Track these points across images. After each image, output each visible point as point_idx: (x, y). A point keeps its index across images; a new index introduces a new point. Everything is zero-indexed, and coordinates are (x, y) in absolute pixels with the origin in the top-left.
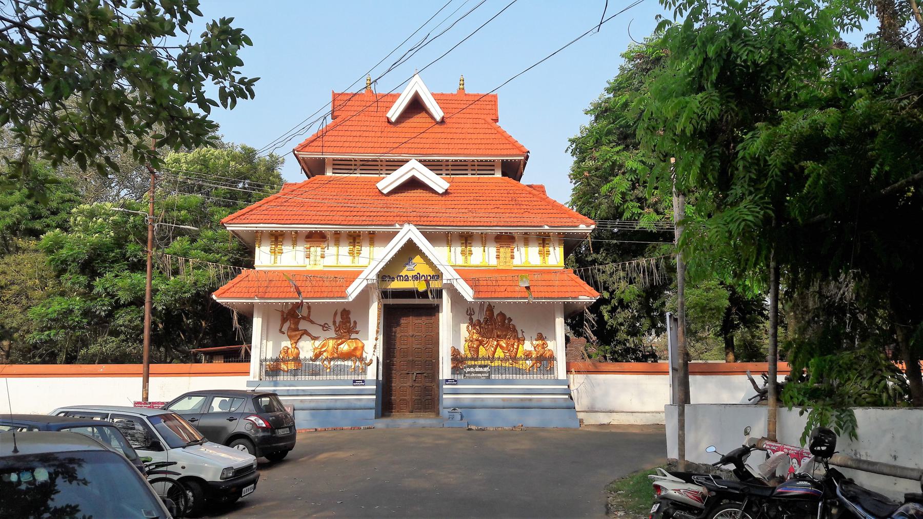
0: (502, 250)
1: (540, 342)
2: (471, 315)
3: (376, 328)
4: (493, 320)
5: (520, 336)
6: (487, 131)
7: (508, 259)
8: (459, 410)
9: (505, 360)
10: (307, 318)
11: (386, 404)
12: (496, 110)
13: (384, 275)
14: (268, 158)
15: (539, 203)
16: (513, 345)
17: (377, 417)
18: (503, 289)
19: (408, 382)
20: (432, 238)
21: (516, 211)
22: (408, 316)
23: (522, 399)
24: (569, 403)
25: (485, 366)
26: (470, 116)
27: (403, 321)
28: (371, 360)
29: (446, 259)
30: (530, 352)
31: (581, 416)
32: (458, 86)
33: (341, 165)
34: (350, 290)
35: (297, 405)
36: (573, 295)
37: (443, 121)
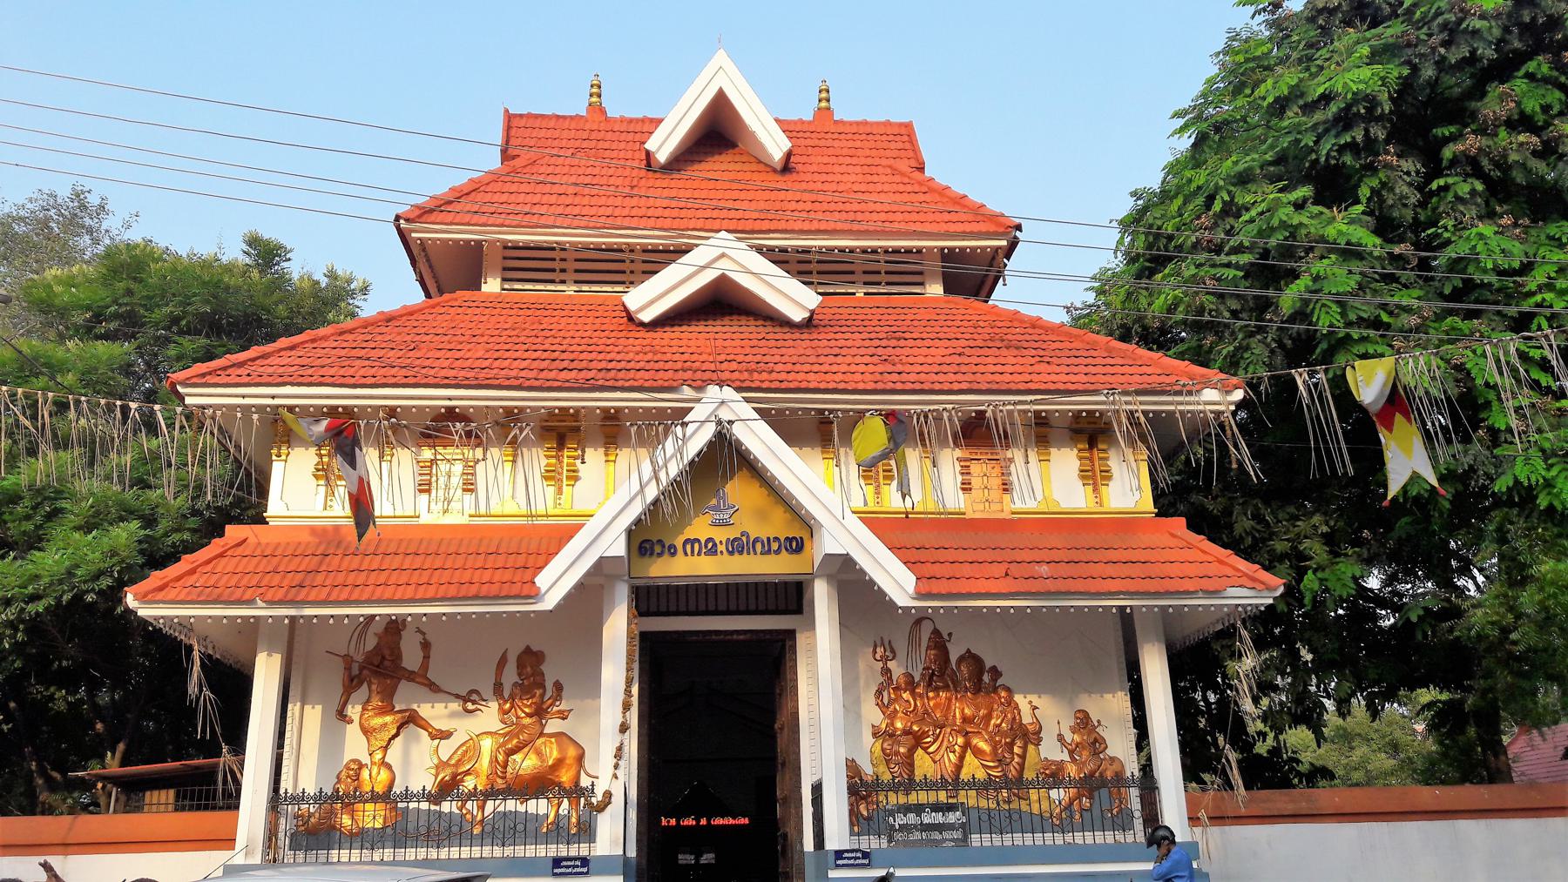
0: (976, 468)
3: (621, 696)
6: (901, 188)
7: (995, 494)
13: (646, 538)
25: (951, 808)
28: (608, 795)
29: (830, 494)
30: (1060, 765)
34: (542, 580)
37: (787, 167)
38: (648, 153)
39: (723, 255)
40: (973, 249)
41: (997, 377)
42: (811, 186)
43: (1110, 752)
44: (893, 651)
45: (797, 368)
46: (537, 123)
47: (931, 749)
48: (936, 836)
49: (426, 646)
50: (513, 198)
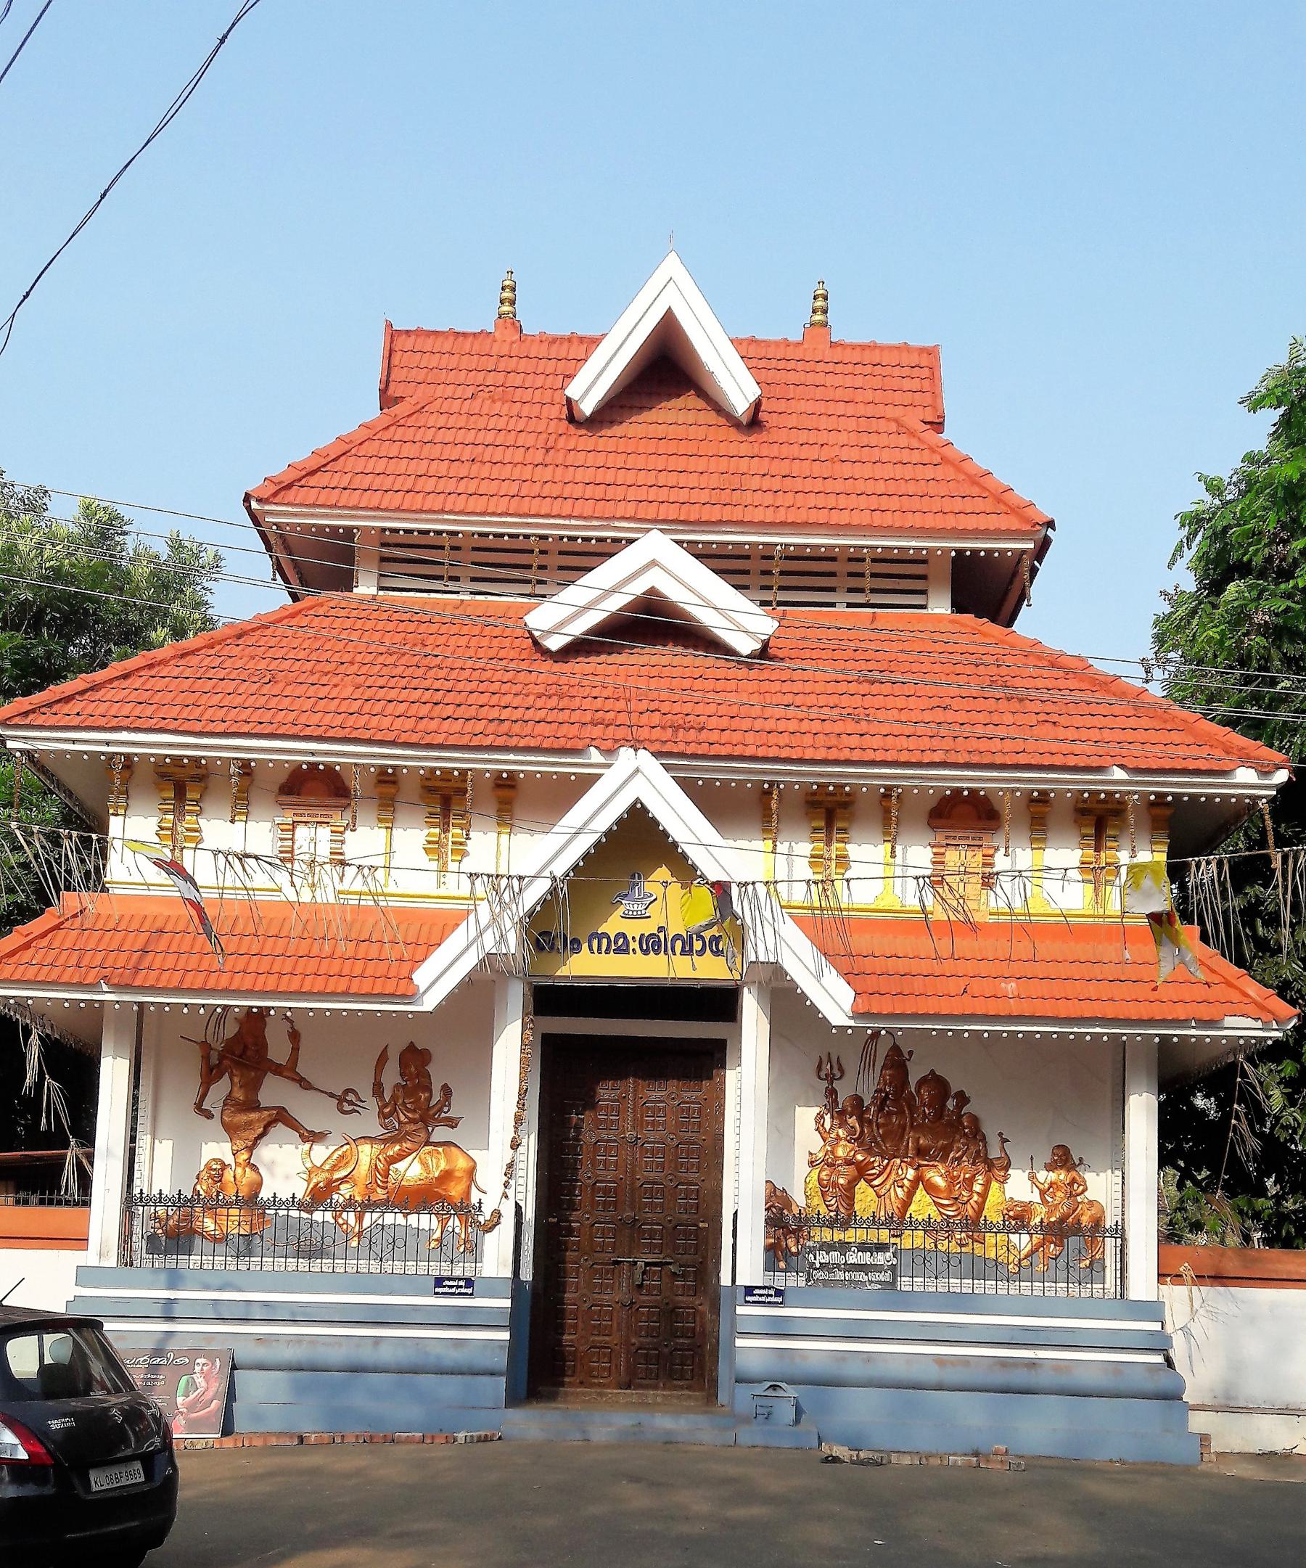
1: (1061, 1176)
2: (830, 1078)
4: (907, 1098)
5: (994, 1153)
6: (906, 455)
8: (791, 1391)
9: (947, 1227)
10: (290, 1072)
11: (544, 1354)
12: (936, 394)
13: (546, 930)
14: (164, 551)
15: (1088, 696)
16: (971, 1181)
17: (514, 1399)
18: (954, 986)
19: (616, 1291)
20: (717, 803)
21: (1008, 718)
22: (620, 1075)
23: (1004, 1363)
24: (1163, 1381)
25: (882, 1247)
26: (850, 409)
27: (606, 1092)
28: (497, 1214)
31: (1199, 1422)
32: (806, 316)
33: (412, 556)
34: (422, 977)
35: (244, 1353)
36: (1205, 1012)
37: (754, 422)
38: (569, 400)
39: (653, 563)
40: (989, 552)
41: (983, 745)
42: (785, 451)
43: (1089, 1195)
44: (841, 1069)
45: (735, 723)
46: (428, 344)
47: (876, 1182)
48: (861, 1276)
49: (295, 1036)
50: (392, 467)
